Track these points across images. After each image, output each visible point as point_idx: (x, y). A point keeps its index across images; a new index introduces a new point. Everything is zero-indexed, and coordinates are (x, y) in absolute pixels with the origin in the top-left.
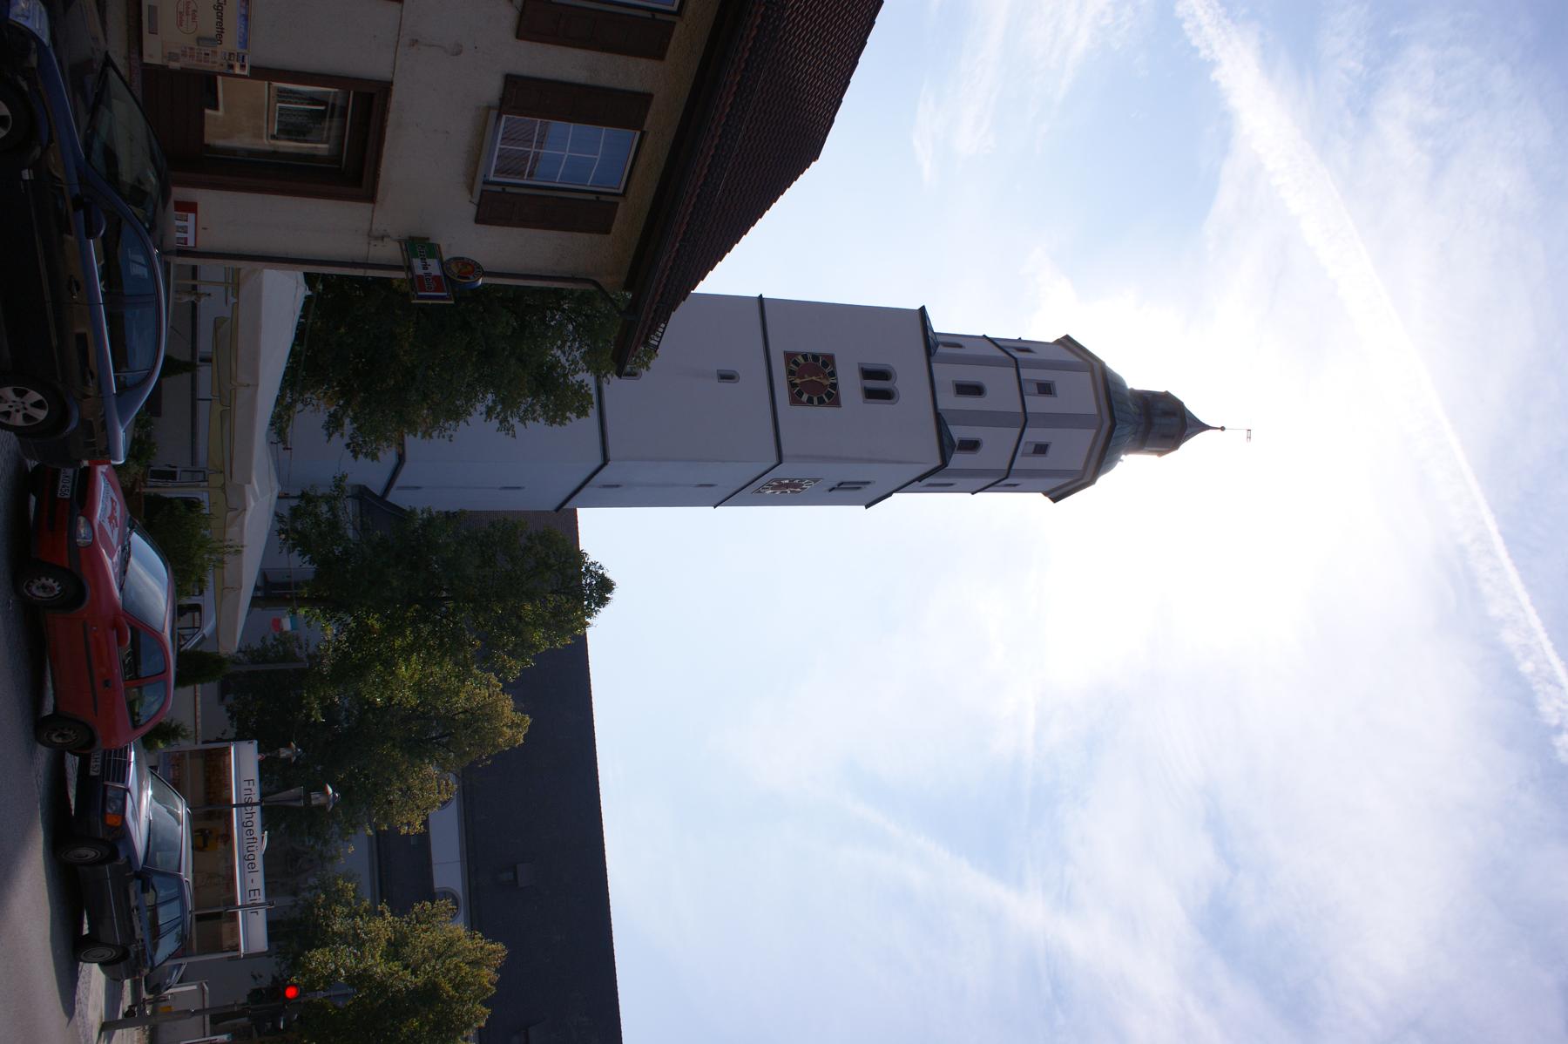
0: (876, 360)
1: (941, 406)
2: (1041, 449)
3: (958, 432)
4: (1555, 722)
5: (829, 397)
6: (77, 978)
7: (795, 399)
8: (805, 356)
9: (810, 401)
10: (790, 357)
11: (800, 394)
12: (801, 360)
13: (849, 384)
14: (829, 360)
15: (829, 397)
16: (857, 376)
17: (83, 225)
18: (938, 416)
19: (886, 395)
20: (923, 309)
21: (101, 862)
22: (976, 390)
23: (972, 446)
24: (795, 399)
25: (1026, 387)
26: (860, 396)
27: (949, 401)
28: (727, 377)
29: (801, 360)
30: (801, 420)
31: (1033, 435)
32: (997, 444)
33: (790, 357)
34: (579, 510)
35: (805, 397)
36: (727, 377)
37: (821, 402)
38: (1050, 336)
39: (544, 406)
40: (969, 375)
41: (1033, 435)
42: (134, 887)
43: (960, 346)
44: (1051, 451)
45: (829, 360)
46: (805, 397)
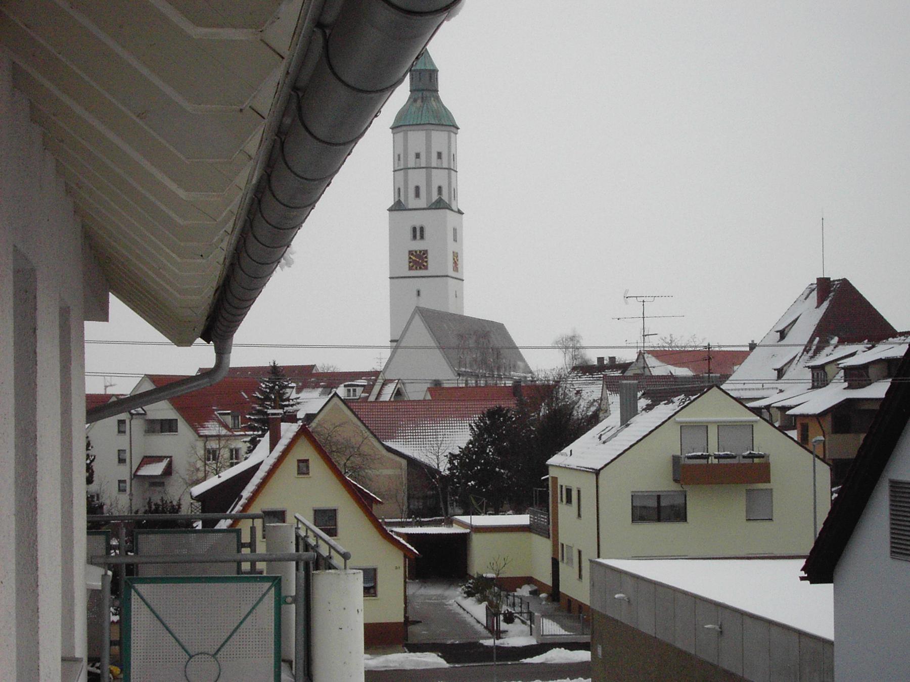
0: (409, 234)
1: (425, 206)
7: (426, 268)
10: (410, 268)
13: (418, 246)
17: (294, 625)
19: (422, 229)
22: (417, 189)
23: (440, 188)
24: (426, 268)
25: (418, 165)
26: (422, 242)
27: (422, 202)
28: (419, 293)
30: (433, 266)
31: (434, 162)
32: (439, 178)
33: (410, 268)
34: (231, 366)
36: (419, 293)
41: (434, 162)
42: (479, 359)
43: (399, 189)
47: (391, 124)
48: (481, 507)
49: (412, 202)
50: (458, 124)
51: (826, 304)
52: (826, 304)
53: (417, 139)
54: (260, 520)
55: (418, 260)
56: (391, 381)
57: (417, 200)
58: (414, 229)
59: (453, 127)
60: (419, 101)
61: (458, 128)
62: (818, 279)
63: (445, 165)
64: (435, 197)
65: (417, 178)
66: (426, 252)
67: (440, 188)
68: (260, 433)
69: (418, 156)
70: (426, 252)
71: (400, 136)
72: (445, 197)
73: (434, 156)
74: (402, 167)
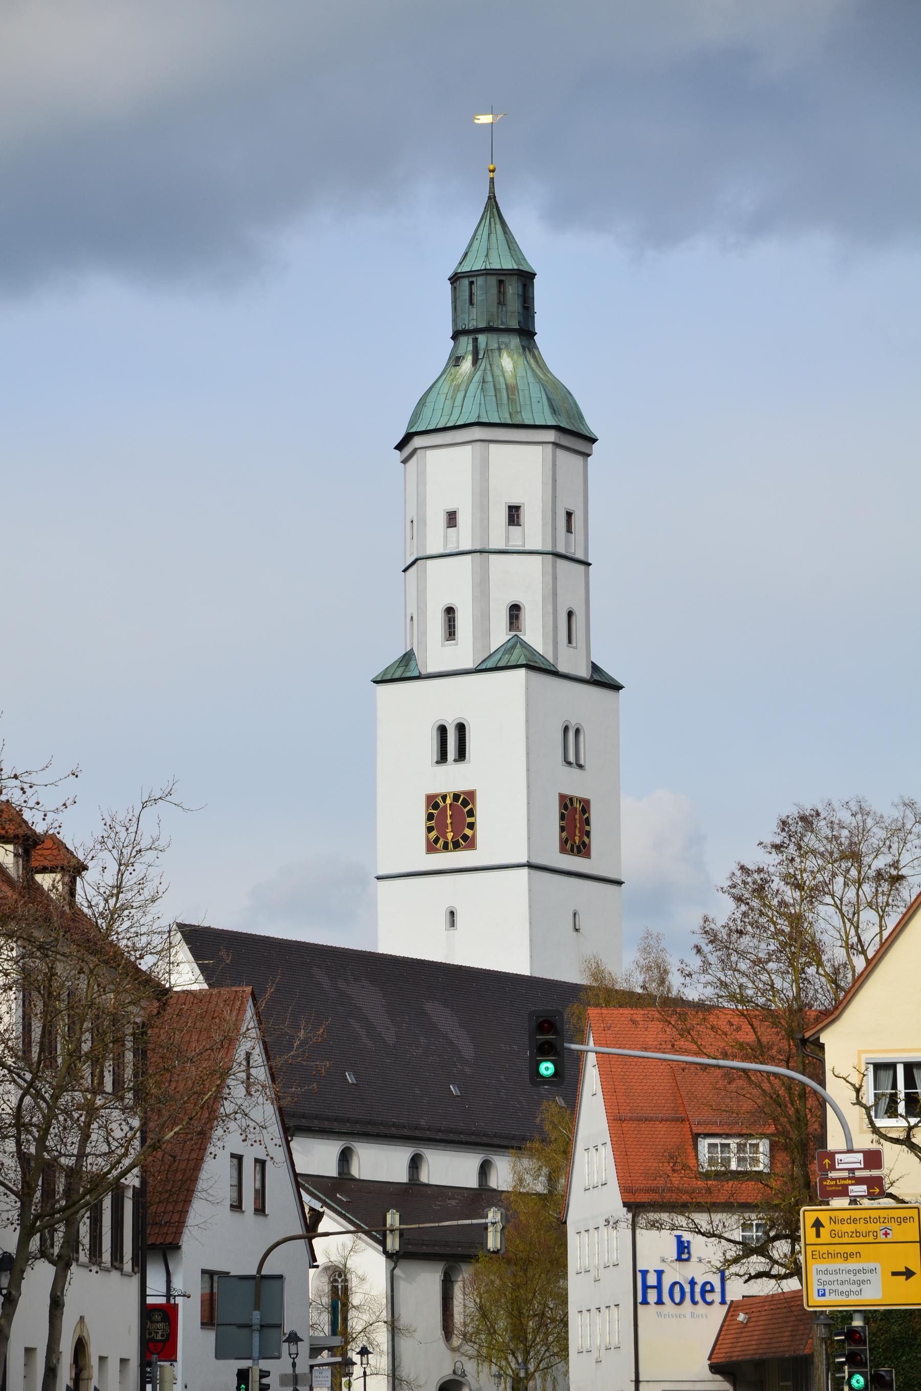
1: (470, 665)
2: (514, 514)
3: (500, 635)
4: (421, 1383)
5: (464, 803)
6: (48, 1346)
8: (430, 829)
9: (471, 826)
10: (431, 847)
11: (465, 838)
12: (433, 834)
13: (452, 779)
14: (433, 802)
15: (464, 803)
16: (443, 768)
18: (477, 671)
20: (396, 448)
21: (56, 1097)
23: (515, 611)
26: (461, 766)
27: (463, 653)
29: (433, 834)
33: (431, 847)
35: (468, 832)
37: (471, 813)
38: (448, 285)
39: (63, 913)
40: (436, 624)
41: (498, 533)
44: (514, 502)
45: (433, 802)
46: (468, 832)
48: (615, 1139)
49: (436, 655)
50: (593, 425)
51: (185, 975)
52: (185, 975)
54: (331, 1170)
56: (876, 1130)
59: (625, 1205)
60: (467, 365)
61: (593, 440)
65: (450, 583)
67: (515, 611)
68: (35, 1056)
69: (452, 519)
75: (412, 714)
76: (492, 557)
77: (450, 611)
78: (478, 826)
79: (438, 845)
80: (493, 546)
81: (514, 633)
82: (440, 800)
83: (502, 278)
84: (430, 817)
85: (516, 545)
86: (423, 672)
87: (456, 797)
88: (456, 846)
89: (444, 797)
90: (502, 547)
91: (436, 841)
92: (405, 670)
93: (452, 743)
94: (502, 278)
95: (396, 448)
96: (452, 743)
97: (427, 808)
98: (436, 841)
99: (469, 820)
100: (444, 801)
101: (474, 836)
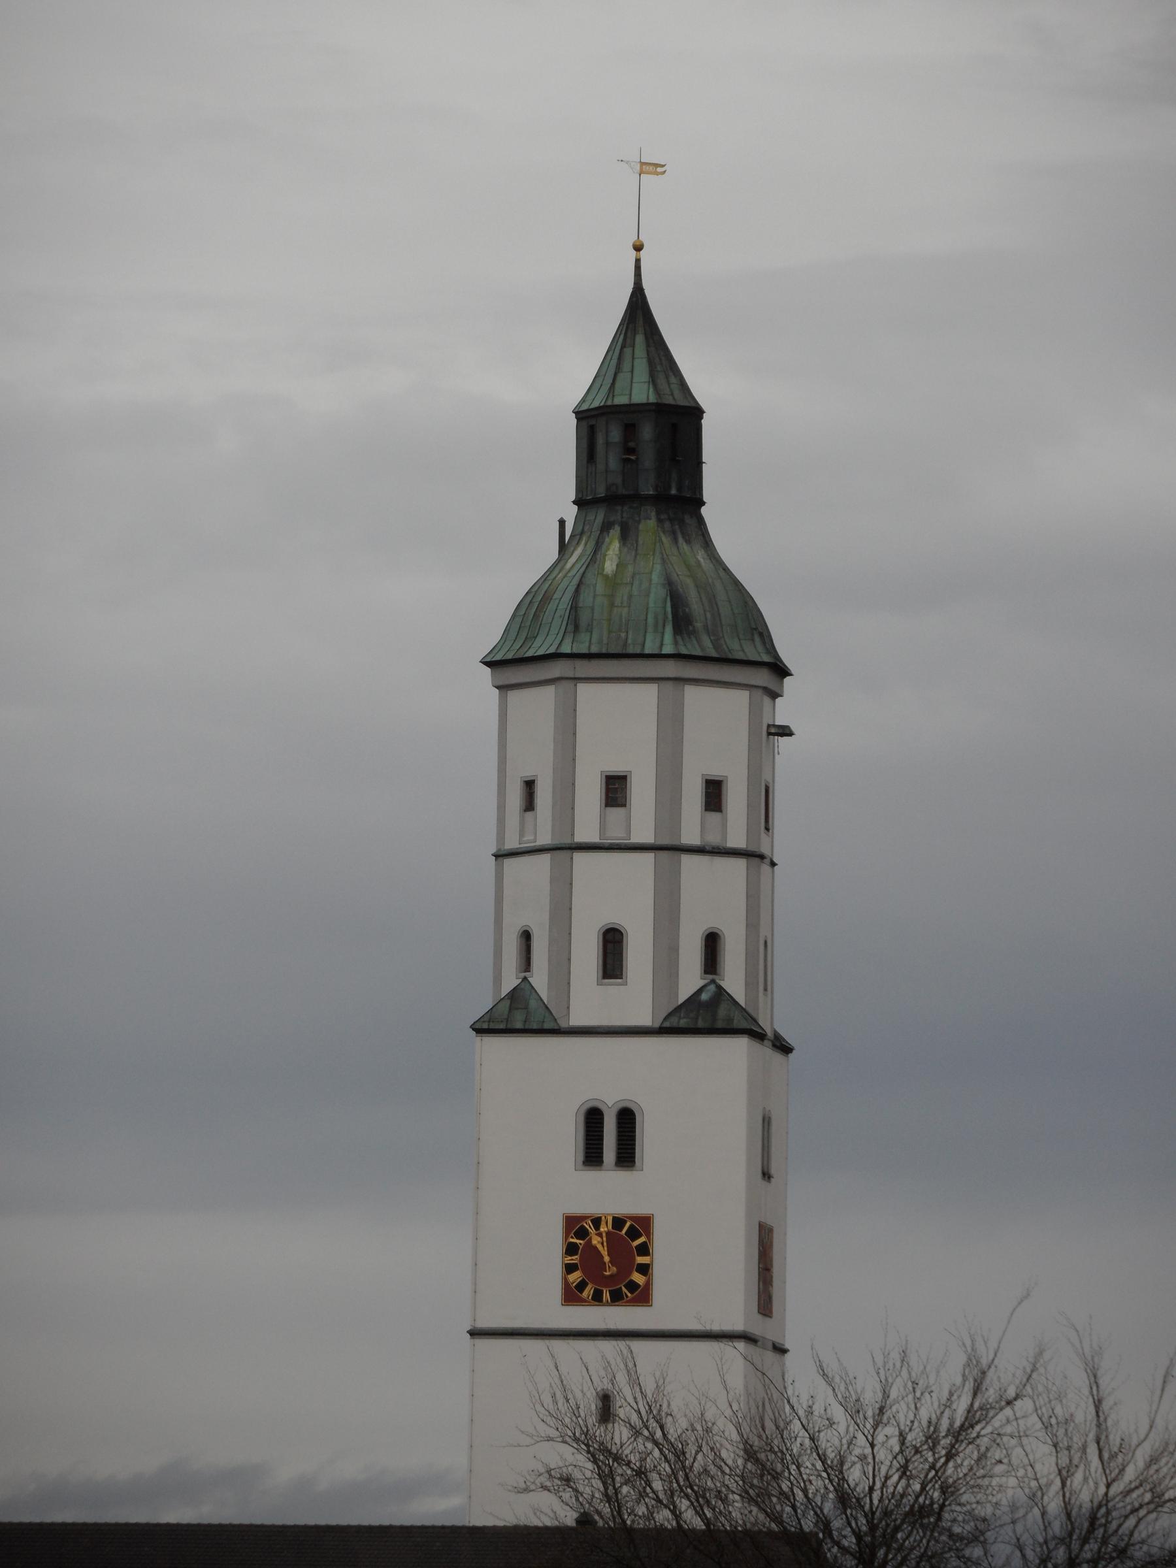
1: (645, 1019)
3: (690, 980)
5: (632, 1234)
7: (642, 1296)
9: (645, 1269)
10: (571, 1296)
11: (632, 1286)
12: (575, 1277)
13: (608, 1193)
15: (632, 1234)
19: (627, 1118)
22: (613, 942)
23: (712, 942)
24: (642, 1296)
25: (713, 839)
26: (623, 1176)
29: (575, 1277)
33: (571, 1296)
35: (588, 1292)
37: (644, 1250)
40: (586, 954)
46: (588, 1292)
47: (490, 633)
49: (589, 1001)
53: (618, 720)
55: (766, 1175)
57: (613, 989)
58: (593, 1118)
61: (781, 671)
62: (574, 502)
63: (737, 839)
64: (690, 980)
65: (615, 891)
66: (641, 1226)
67: (712, 942)
70: (641, 1226)
71: (537, 706)
72: (733, 981)
73: (589, 793)
74: (545, 839)
75: (548, 1083)
76: (687, 860)
77: (526, 936)
78: (657, 1271)
79: (585, 1294)
80: (581, 837)
81: (711, 977)
82: (589, 1225)
83: (593, 422)
84: (571, 1249)
85: (616, 835)
86: (563, 1024)
87: (618, 1222)
88: (617, 1298)
89: (597, 1222)
90: (595, 839)
91: (581, 1286)
92: (518, 1016)
93: (610, 1136)
94: (593, 422)
95: (791, 734)
96: (610, 1136)
97: (632, 1218)
98: (581, 1286)
99: (641, 1260)
100: (597, 1227)
101: (648, 1284)
